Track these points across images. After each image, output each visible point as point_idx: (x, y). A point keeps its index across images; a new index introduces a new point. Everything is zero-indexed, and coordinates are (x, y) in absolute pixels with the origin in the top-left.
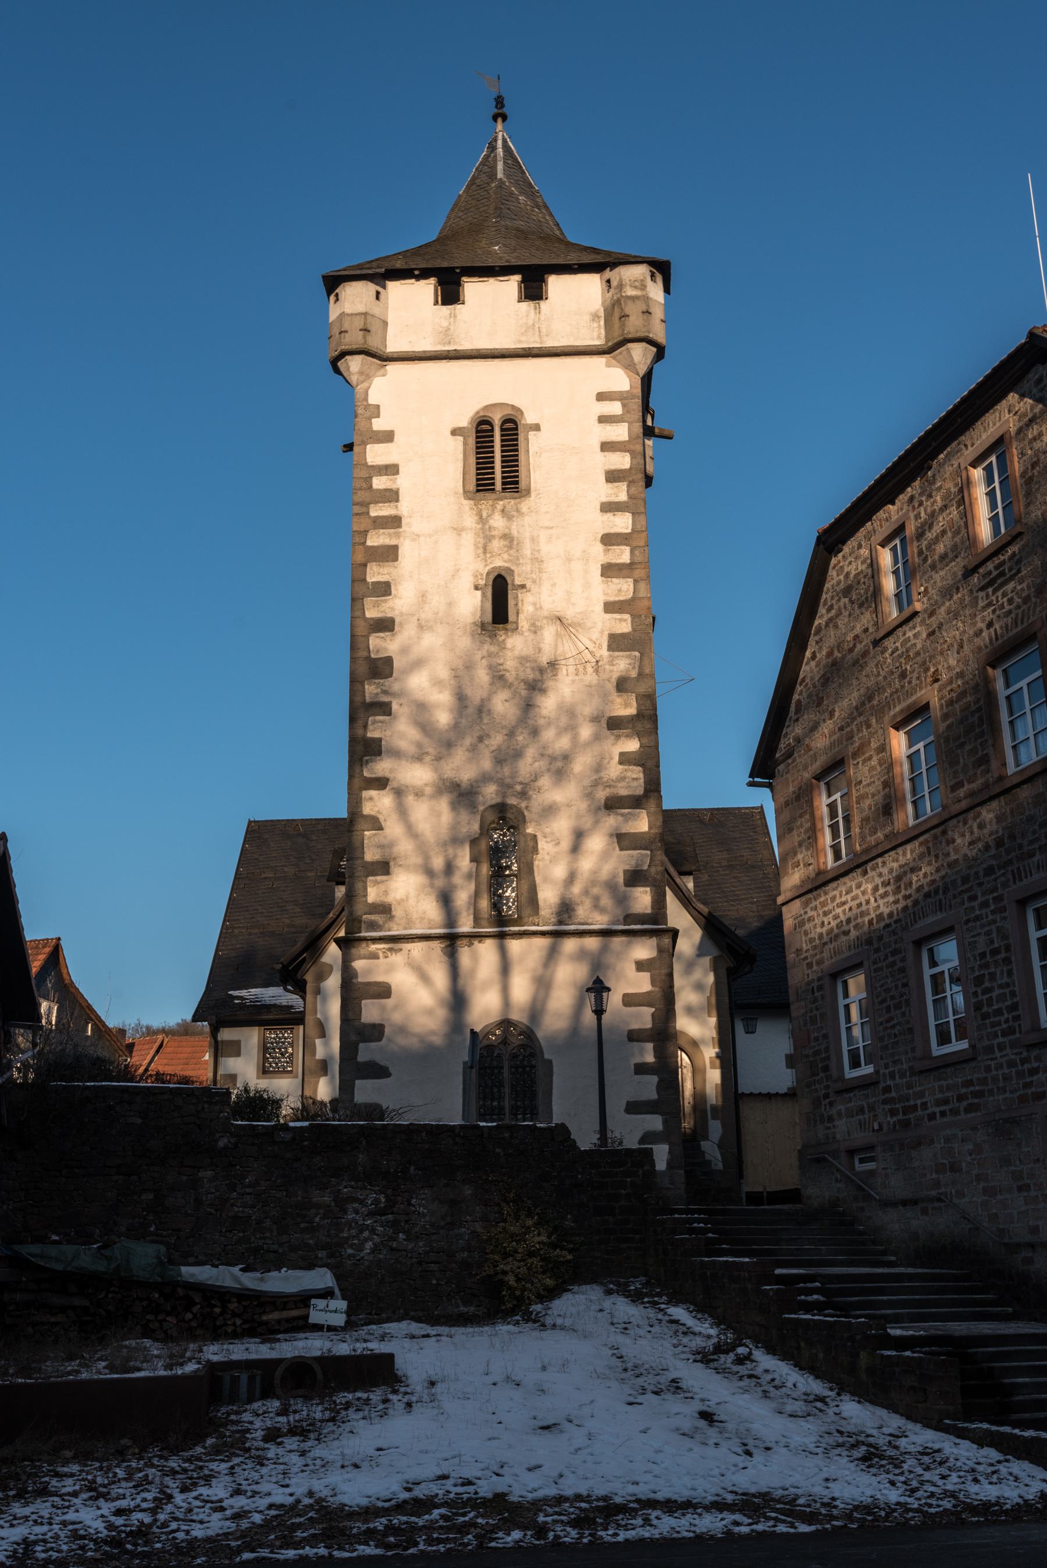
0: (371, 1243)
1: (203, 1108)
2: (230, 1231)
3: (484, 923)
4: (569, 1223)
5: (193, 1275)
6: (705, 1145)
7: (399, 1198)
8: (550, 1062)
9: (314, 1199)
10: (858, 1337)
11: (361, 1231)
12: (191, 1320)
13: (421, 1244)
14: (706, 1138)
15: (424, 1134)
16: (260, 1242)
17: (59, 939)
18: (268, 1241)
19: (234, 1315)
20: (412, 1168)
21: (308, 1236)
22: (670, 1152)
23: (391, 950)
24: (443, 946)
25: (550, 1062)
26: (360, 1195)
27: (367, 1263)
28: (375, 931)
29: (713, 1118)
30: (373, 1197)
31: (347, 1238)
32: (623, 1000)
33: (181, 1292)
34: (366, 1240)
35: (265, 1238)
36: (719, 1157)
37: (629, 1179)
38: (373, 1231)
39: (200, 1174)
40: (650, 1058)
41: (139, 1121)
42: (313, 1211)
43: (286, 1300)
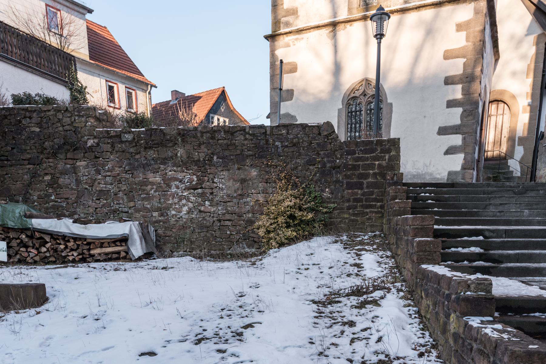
0: (186, 207)
1: (75, 120)
2: (99, 199)
3: (355, 11)
4: (327, 194)
5: (39, 225)
6: (511, 162)
7: (206, 178)
8: (391, 104)
9: (150, 179)
10: (453, 296)
11: (181, 200)
12: (45, 252)
13: (220, 208)
14: (512, 157)
15: (222, 133)
16: (117, 207)
17: (224, 87)
18: (121, 206)
19: (72, 250)
20: (215, 157)
21: (146, 203)
22: (465, 159)
23: (297, 39)
24: (328, 31)
25: (391, 104)
26: (180, 176)
27: (184, 220)
28: (288, 27)
29: (519, 145)
30: (189, 177)
31: (171, 204)
32: (444, 55)
33: (37, 235)
34: (184, 205)
35: (119, 204)
36: (519, 169)
37: (377, 163)
38: (188, 200)
39: (78, 164)
40: (459, 95)
41: (38, 130)
42: (149, 187)
43: (102, 241)
